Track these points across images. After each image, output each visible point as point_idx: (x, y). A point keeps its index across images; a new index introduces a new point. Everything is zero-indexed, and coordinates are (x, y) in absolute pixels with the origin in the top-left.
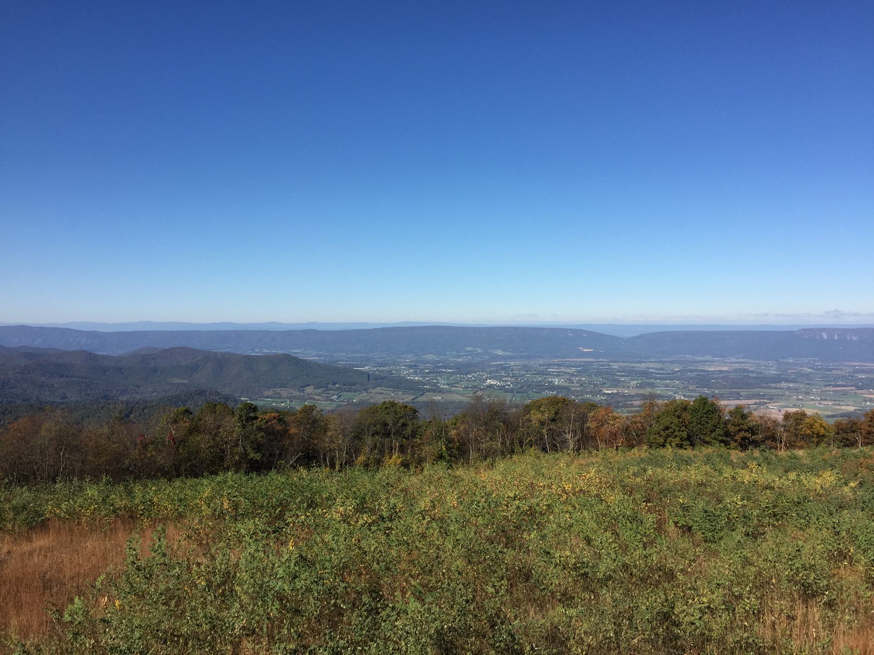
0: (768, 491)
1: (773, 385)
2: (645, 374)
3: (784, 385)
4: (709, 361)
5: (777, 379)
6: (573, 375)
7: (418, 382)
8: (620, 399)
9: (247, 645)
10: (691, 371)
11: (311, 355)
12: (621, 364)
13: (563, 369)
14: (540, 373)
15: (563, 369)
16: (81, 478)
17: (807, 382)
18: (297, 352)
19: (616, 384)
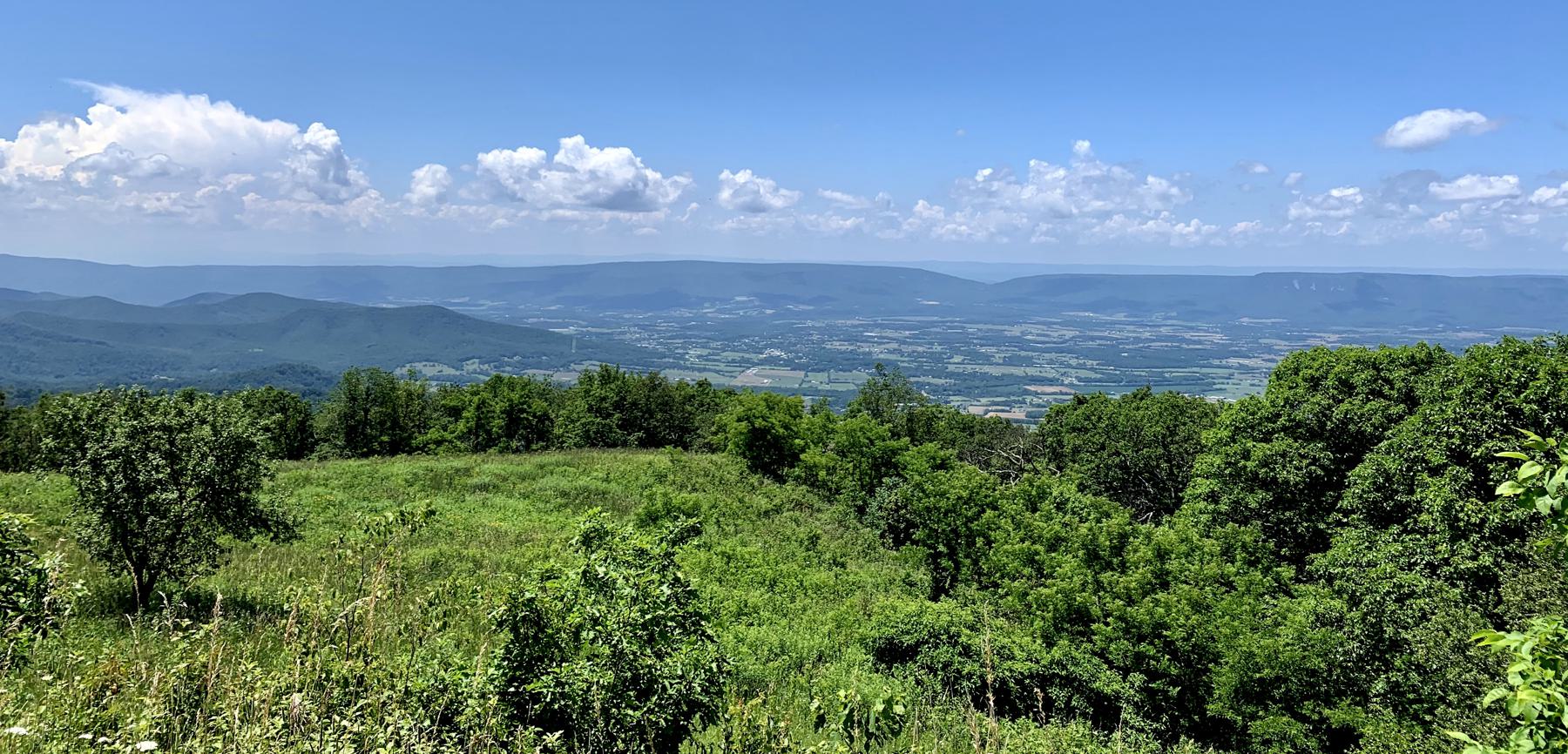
0: (584, 634)
1: (1216, 362)
2: (1019, 342)
3: (1233, 361)
4: (1120, 323)
5: (1224, 352)
6: (905, 343)
7: (654, 353)
8: (977, 383)
9: (1564, 676)
10: (1093, 339)
11: (485, 307)
12: (981, 326)
13: (889, 333)
14: (851, 339)
15: (889, 333)
16: (1107, 490)
17: (1267, 356)
18: (458, 303)
19: (975, 357)
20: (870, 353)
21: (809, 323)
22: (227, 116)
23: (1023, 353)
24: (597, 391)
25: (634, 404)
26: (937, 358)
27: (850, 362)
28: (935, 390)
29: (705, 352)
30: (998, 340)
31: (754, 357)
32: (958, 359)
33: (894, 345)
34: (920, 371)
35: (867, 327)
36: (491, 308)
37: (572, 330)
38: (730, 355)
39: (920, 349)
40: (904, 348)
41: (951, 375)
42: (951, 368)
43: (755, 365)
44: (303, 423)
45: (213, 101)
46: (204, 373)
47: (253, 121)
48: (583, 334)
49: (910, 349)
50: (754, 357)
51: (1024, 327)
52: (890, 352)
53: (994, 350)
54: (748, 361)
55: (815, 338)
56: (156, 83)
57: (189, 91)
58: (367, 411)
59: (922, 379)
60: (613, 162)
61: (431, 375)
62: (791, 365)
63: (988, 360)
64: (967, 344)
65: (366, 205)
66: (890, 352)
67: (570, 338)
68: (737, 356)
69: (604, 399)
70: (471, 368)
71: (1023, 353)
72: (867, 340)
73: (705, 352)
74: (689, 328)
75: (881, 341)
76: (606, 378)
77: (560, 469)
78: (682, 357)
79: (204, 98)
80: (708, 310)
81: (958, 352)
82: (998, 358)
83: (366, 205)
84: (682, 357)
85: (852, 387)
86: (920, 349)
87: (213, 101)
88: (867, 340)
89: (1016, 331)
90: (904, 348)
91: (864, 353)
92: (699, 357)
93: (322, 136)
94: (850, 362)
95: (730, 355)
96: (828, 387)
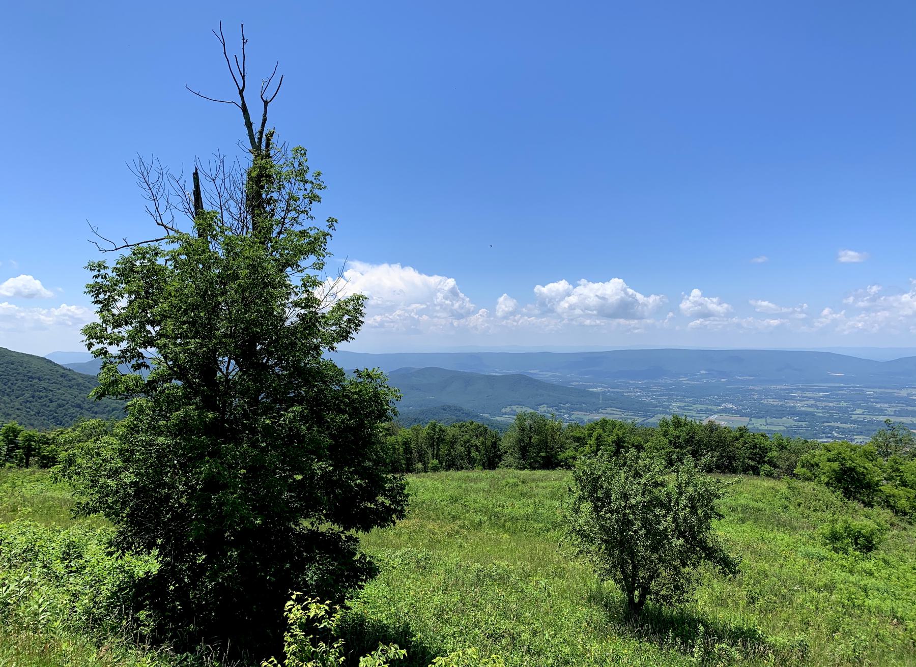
6: (820, 400)
8: (874, 427)
12: (875, 390)
13: (808, 394)
14: (780, 398)
15: (808, 394)
18: (536, 373)
20: (795, 407)
21: (751, 387)
22: (411, 275)
23: (909, 408)
24: (673, 432)
25: (700, 441)
26: (844, 411)
27: (780, 413)
28: (843, 431)
29: (682, 404)
30: (890, 399)
31: (715, 408)
32: (859, 411)
33: (813, 402)
34: (831, 418)
35: (792, 390)
36: (551, 376)
37: (598, 389)
38: (699, 407)
39: (831, 405)
40: (819, 404)
41: (855, 422)
42: (854, 417)
43: (715, 413)
44: (495, 443)
45: (403, 267)
46: (405, 409)
47: (424, 277)
48: (606, 392)
49: (824, 404)
50: (715, 408)
51: (909, 391)
52: (809, 406)
53: (886, 405)
54: (711, 410)
55: (755, 397)
56: (375, 258)
57: (391, 262)
58: (530, 438)
59: (833, 424)
60: (612, 289)
61: (566, 419)
62: (737, 412)
63: (881, 411)
64: (867, 402)
65: (478, 319)
66: (809, 406)
67: (598, 394)
68: (703, 407)
69: (678, 437)
70: (543, 410)
71: (909, 408)
72: (792, 398)
73: (682, 404)
74: (671, 390)
75: (802, 399)
76: (678, 424)
77: (508, 474)
78: (668, 407)
79: (398, 266)
80: (683, 380)
81: (859, 407)
82: (890, 411)
83: (478, 319)
84: (668, 407)
85: (783, 428)
86: (831, 405)
87: (403, 267)
88: (792, 398)
89: (904, 393)
90: (819, 404)
91: (791, 407)
92: (678, 407)
93: (451, 282)
94: (780, 413)
95: (699, 407)
96: (766, 428)
